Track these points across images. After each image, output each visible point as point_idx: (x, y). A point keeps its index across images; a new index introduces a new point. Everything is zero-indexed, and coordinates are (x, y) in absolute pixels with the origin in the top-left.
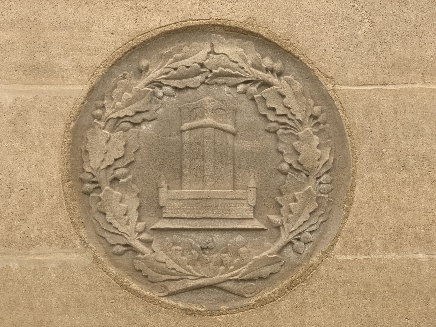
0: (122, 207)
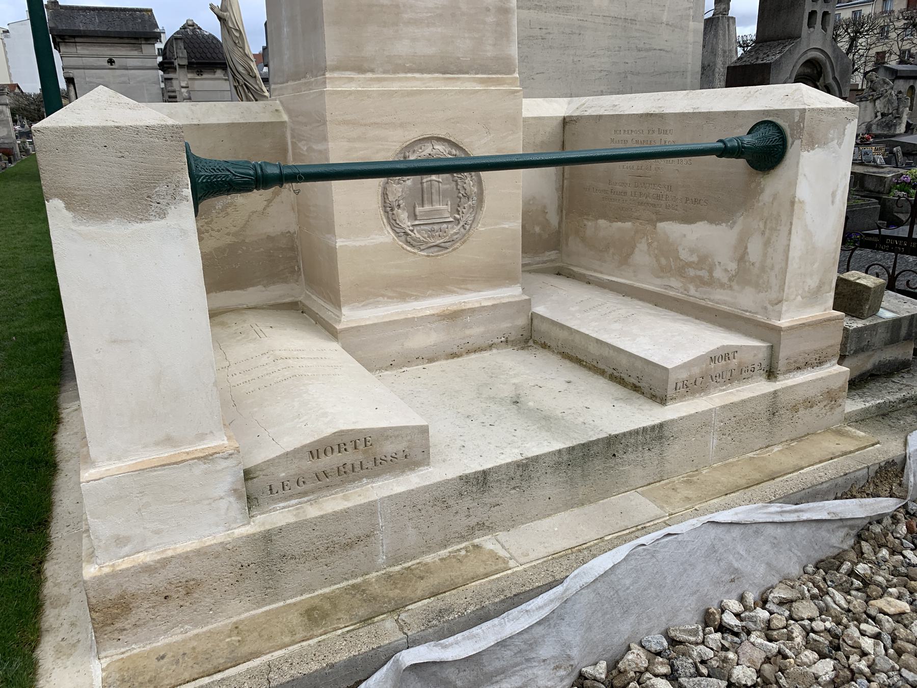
0: (403, 215)
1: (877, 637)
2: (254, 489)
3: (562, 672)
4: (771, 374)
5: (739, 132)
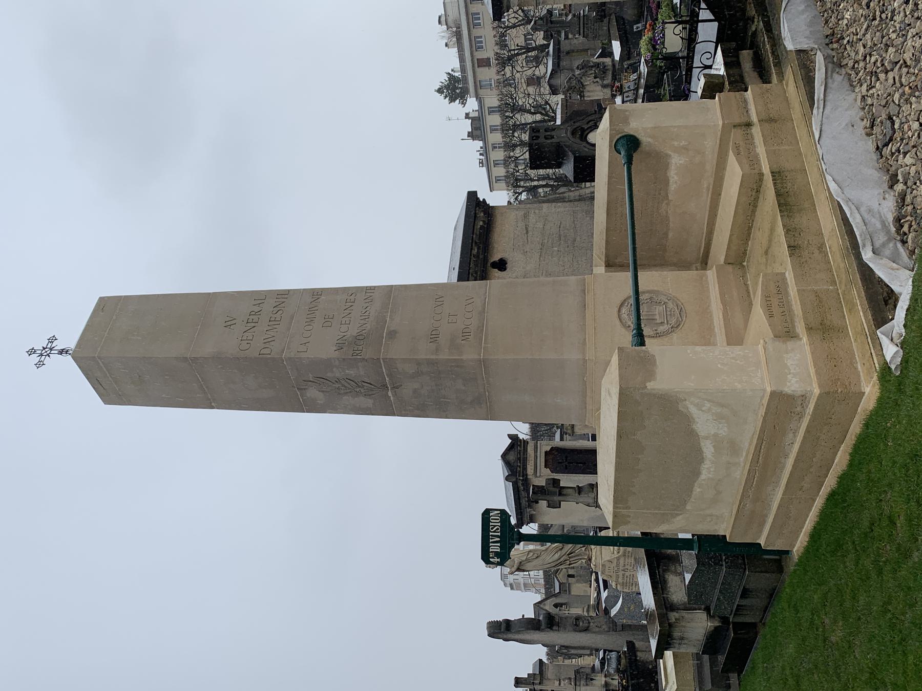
0: (661, 329)
1: (871, 55)
2: (787, 334)
3: (887, 196)
4: (749, 125)
5: (622, 159)
